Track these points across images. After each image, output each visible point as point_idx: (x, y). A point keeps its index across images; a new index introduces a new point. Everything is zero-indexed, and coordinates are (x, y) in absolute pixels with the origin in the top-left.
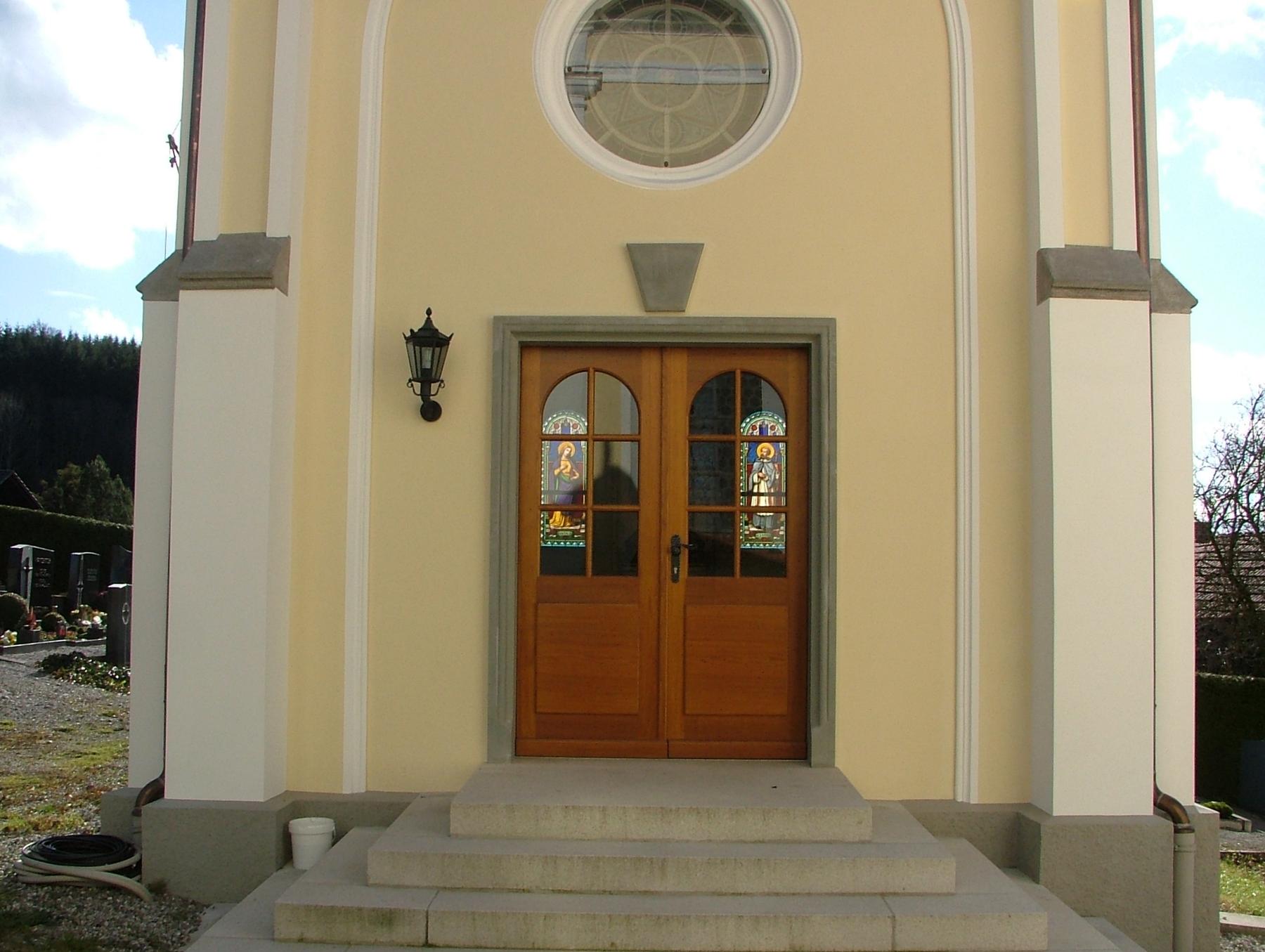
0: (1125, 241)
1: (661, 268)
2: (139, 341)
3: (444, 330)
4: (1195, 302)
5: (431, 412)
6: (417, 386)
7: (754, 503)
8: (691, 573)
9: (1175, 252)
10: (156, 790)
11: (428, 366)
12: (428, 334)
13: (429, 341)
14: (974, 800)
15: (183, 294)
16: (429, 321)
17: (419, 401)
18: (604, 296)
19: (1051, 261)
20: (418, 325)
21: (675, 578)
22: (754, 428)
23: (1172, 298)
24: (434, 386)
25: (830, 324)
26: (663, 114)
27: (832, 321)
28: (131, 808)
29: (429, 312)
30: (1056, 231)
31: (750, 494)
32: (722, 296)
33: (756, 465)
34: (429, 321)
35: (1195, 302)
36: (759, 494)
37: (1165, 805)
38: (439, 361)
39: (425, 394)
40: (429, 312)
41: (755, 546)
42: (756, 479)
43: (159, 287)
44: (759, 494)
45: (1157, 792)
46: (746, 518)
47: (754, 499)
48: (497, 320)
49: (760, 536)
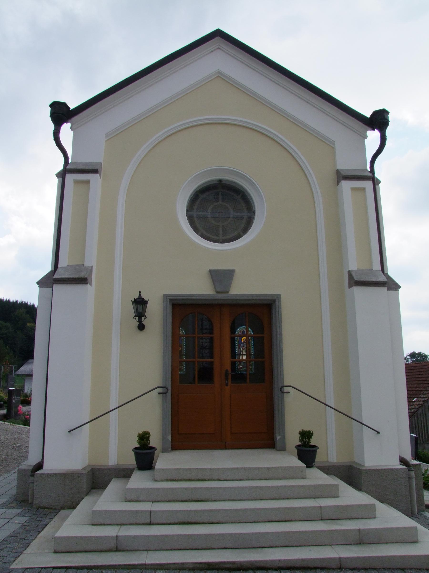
0: (138, 305)
1: (221, 277)
2: (36, 305)
3: (146, 299)
4: (399, 287)
5: (141, 327)
6: (137, 318)
7: (241, 358)
8: (232, 383)
9: (393, 270)
10: (40, 466)
11: (141, 311)
12: (139, 300)
13: (140, 303)
14: (335, 461)
15: (55, 286)
16: (140, 295)
17: (138, 323)
18: (198, 287)
19: (353, 274)
20: (136, 297)
21: (227, 385)
22: (240, 332)
23: (392, 286)
24: (143, 318)
25: (279, 296)
26: (219, 226)
27: (279, 295)
28: (29, 473)
29: (140, 292)
30: (354, 264)
31: (240, 355)
32: (244, 287)
33: (242, 345)
34: (140, 295)
35: (399, 287)
36: (243, 355)
37: (403, 461)
38: (144, 309)
39: (140, 321)
40: (140, 292)
41: (242, 373)
42: (242, 349)
43: (48, 282)
44: (243, 355)
45: (400, 456)
46: (238, 363)
47: (241, 357)
48: (165, 295)
49: (243, 369)
